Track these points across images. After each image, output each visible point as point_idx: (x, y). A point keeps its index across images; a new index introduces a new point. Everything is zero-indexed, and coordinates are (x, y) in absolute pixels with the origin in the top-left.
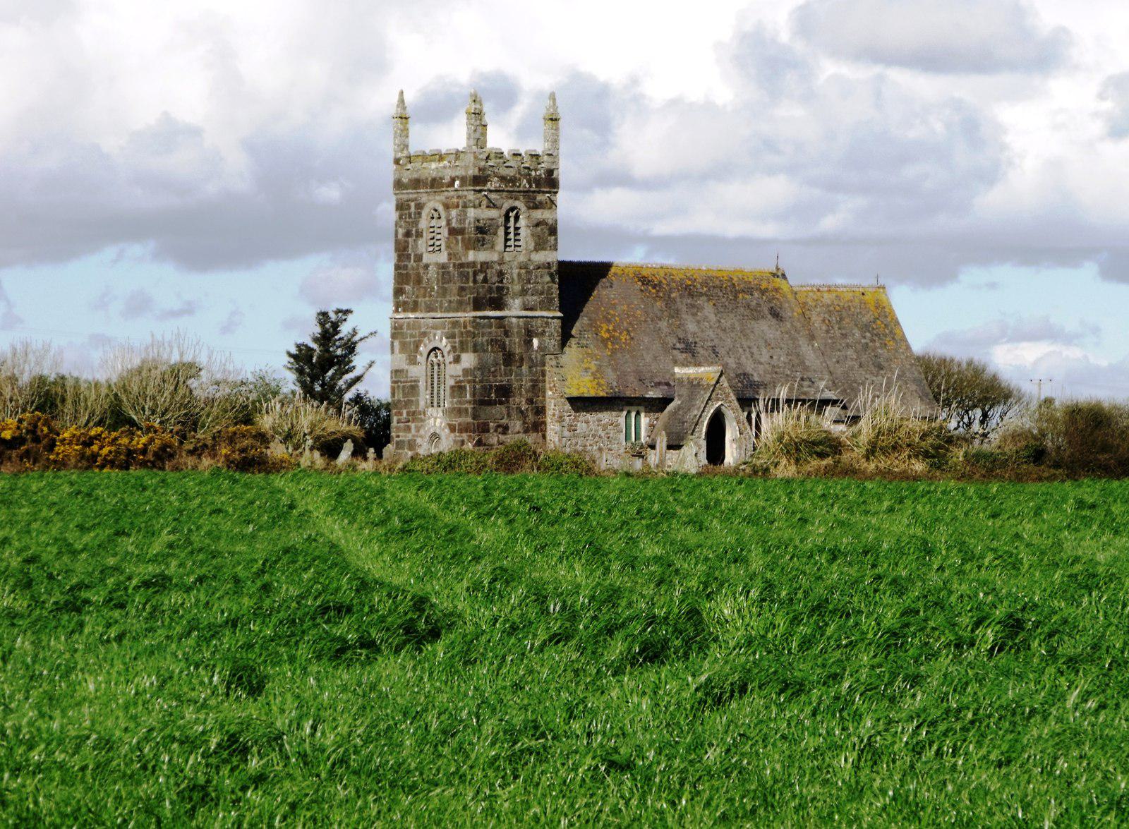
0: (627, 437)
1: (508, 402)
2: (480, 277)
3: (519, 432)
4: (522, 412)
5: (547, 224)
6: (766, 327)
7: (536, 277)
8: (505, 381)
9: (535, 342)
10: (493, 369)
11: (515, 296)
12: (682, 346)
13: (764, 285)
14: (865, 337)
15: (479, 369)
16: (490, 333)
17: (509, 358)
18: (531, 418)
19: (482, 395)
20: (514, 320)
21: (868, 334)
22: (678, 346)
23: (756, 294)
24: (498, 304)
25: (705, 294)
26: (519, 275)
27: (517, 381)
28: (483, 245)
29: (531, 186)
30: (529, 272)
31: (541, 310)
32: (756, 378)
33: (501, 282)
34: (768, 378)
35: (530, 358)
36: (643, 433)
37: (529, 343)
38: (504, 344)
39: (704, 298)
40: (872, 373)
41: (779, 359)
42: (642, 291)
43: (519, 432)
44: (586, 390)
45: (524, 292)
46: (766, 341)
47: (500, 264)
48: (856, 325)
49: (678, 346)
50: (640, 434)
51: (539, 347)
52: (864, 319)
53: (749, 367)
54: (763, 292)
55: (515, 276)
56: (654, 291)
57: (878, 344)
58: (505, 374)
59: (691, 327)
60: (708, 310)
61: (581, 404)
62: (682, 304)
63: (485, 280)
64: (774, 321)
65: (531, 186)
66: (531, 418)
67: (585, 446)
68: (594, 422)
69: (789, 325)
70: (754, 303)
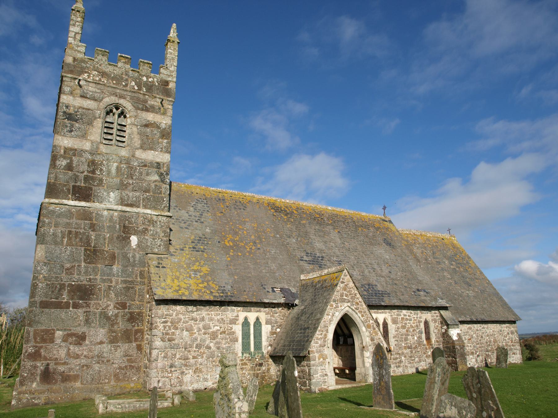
0: (246, 347)
1: (88, 306)
2: (63, 163)
3: (101, 343)
4: (108, 318)
5: (158, 127)
6: (382, 251)
7: (141, 173)
8: (83, 280)
9: (134, 240)
10: (68, 265)
11: (111, 188)
12: (310, 258)
13: (377, 225)
14: (452, 265)
15: (45, 264)
16: (68, 224)
17: (93, 254)
18: (122, 325)
19: (46, 295)
20: (105, 213)
21: (454, 263)
22: (305, 258)
23: (372, 229)
24: (84, 193)
25: (331, 225)
26: (118, 169)
27: (104, 281)
28: (71, 131)
29: (140, 89)
30: (130, 168)
31: (145, 207)
32: (379, 288)
33: (93, 172)
34: (389, 289)
35: (125, 257)
36: (265, 343)
37: (126, 240)
38: (88, 238)
39: (331, 227)
40: (464, 288)
41: (396, 275)
42: (274, 215)
43: (101, 343)
44: (187, 293)
45: (122, 186)
46: (384, 261)
47: (92, 154)
48: (445, 257)
49: (305, 258)
50: (260, 343)
51: (138, 245)
52: (448, 254)
53: (373, 279)
54: (378, 229)
55: (113, 170)
56: (286, 217)
57: (462, 269)
58: (86, 273)
59: (319, 245)
60: (334, 235)
61: (426, 323)
62: (312, 229)
63: (69, 167)
64: (388, 247)
65: (140, 89)
66: (122, 325)
67: (187, 359)
68: (199, 330)
69: (399, 251)
70: (371, 234)
